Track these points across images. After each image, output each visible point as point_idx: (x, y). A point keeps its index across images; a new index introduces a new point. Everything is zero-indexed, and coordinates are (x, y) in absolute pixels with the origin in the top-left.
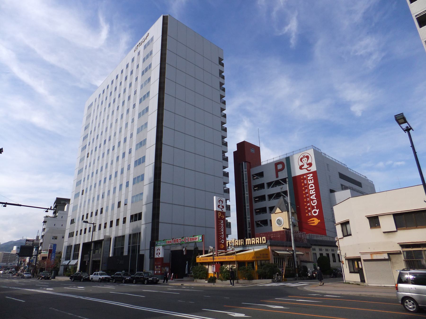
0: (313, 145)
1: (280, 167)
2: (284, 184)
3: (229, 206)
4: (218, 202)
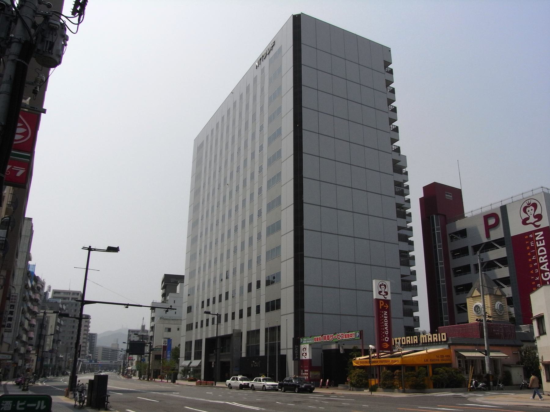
0: (543, 186)
1: (492, 222)
2: (499, 248)
4: (379, 286)
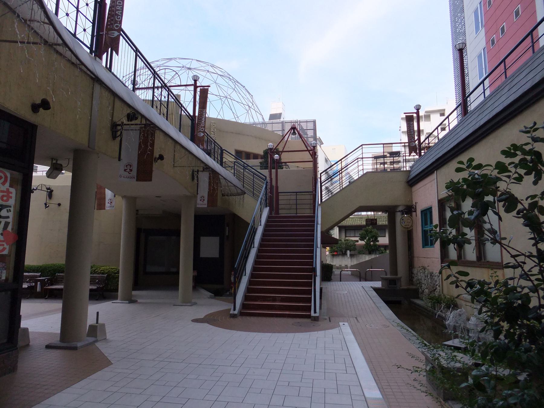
3: (323, 261)
